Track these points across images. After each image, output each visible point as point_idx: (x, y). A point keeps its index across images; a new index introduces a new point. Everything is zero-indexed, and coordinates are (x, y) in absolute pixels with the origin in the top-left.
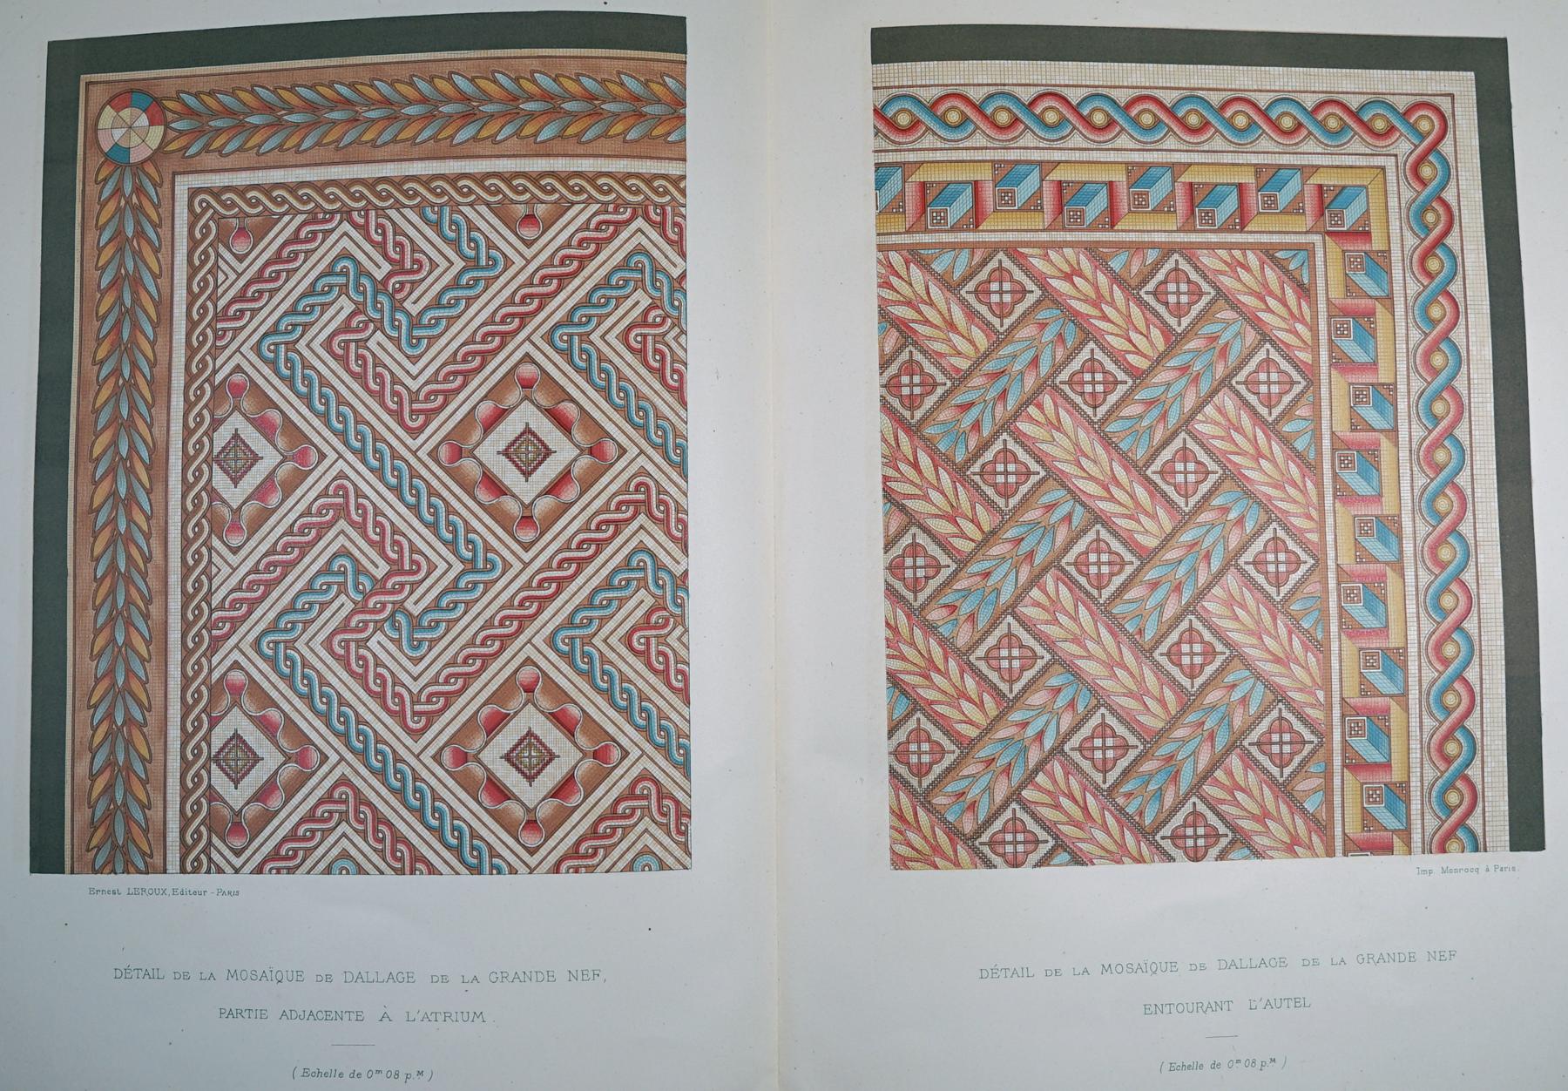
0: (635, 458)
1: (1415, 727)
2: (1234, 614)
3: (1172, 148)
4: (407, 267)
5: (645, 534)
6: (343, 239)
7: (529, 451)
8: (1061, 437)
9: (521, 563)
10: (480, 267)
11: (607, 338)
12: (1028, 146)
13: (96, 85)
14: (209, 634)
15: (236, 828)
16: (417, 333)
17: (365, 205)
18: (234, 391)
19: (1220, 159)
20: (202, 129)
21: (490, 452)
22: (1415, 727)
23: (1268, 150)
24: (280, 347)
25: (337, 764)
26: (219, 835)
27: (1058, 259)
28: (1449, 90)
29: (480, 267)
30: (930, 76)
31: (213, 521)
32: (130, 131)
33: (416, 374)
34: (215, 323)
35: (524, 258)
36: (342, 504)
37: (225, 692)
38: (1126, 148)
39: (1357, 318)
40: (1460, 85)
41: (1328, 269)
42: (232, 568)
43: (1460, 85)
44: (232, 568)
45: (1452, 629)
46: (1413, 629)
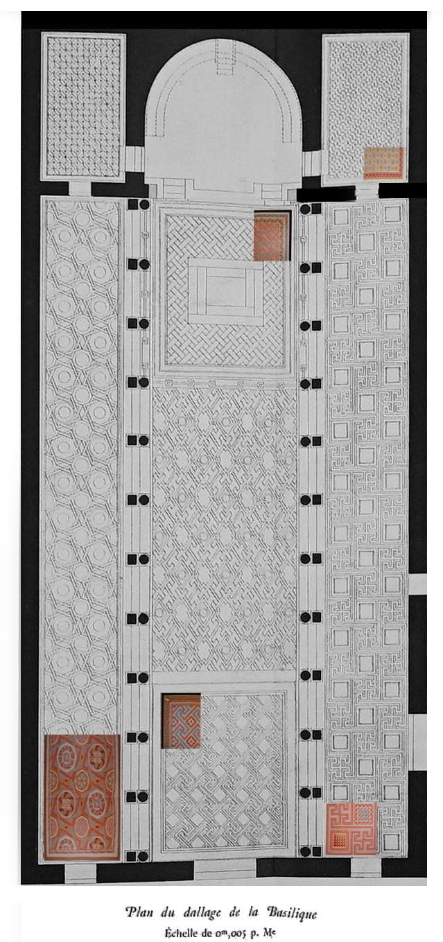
0: (198, 722)
1: (284, 254)
2: (273, 246)
3: (271, 218)
4: (184, 709)
5: (198, 727)
6: (180, 708)
7: (191, 722)
8: (264, 236)
9: (191, 729)
10: (188, 709)
11: (196, 715)
12: (263, 218)
13: (165, 696)
14: (172, 733)
15: (174, 746)
16: (185, 714)
17: (182, 705)
18: (174, 717)
19: (274, 218)
20: (171, 700)
21: (189, 722)
22: (284, 254)
23: (277, 218)
24: (176, 714)
25: (180, 742)
26: (173, 746)
27: (264, 224)
28: (289, 208)
29: (188, 709)
30: (257, 213)
31: (173, 726)
32: (167, 700)
33: (185, 716)
34: (173, 713)
35: (191, 709)
36: (180, 725)
37: (173, 737)
38: (268, 218)
39: (282, 228)
40: (288, 214)
41: (280, 225)
42: (174, 729)
43: (288, 214)
44: (174, 729)
45: (286, 247)
46: (284, 247)
